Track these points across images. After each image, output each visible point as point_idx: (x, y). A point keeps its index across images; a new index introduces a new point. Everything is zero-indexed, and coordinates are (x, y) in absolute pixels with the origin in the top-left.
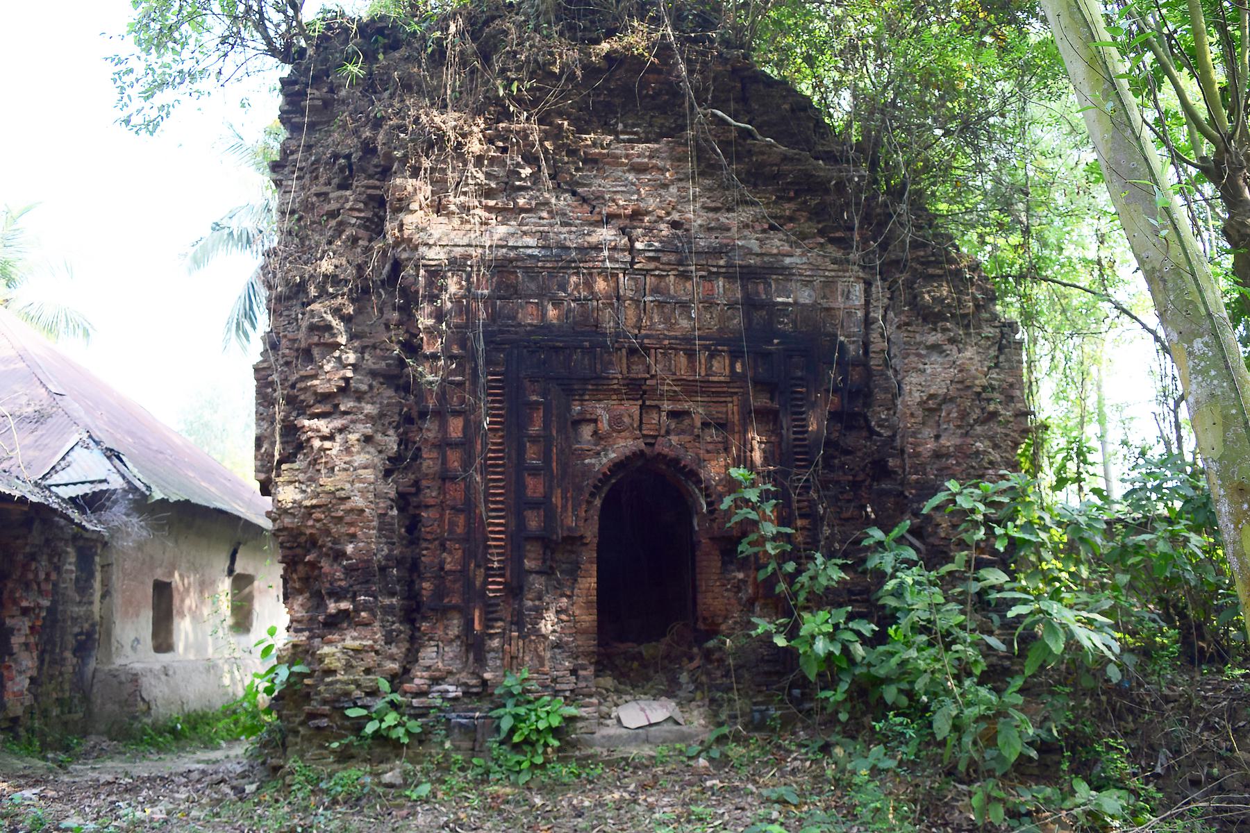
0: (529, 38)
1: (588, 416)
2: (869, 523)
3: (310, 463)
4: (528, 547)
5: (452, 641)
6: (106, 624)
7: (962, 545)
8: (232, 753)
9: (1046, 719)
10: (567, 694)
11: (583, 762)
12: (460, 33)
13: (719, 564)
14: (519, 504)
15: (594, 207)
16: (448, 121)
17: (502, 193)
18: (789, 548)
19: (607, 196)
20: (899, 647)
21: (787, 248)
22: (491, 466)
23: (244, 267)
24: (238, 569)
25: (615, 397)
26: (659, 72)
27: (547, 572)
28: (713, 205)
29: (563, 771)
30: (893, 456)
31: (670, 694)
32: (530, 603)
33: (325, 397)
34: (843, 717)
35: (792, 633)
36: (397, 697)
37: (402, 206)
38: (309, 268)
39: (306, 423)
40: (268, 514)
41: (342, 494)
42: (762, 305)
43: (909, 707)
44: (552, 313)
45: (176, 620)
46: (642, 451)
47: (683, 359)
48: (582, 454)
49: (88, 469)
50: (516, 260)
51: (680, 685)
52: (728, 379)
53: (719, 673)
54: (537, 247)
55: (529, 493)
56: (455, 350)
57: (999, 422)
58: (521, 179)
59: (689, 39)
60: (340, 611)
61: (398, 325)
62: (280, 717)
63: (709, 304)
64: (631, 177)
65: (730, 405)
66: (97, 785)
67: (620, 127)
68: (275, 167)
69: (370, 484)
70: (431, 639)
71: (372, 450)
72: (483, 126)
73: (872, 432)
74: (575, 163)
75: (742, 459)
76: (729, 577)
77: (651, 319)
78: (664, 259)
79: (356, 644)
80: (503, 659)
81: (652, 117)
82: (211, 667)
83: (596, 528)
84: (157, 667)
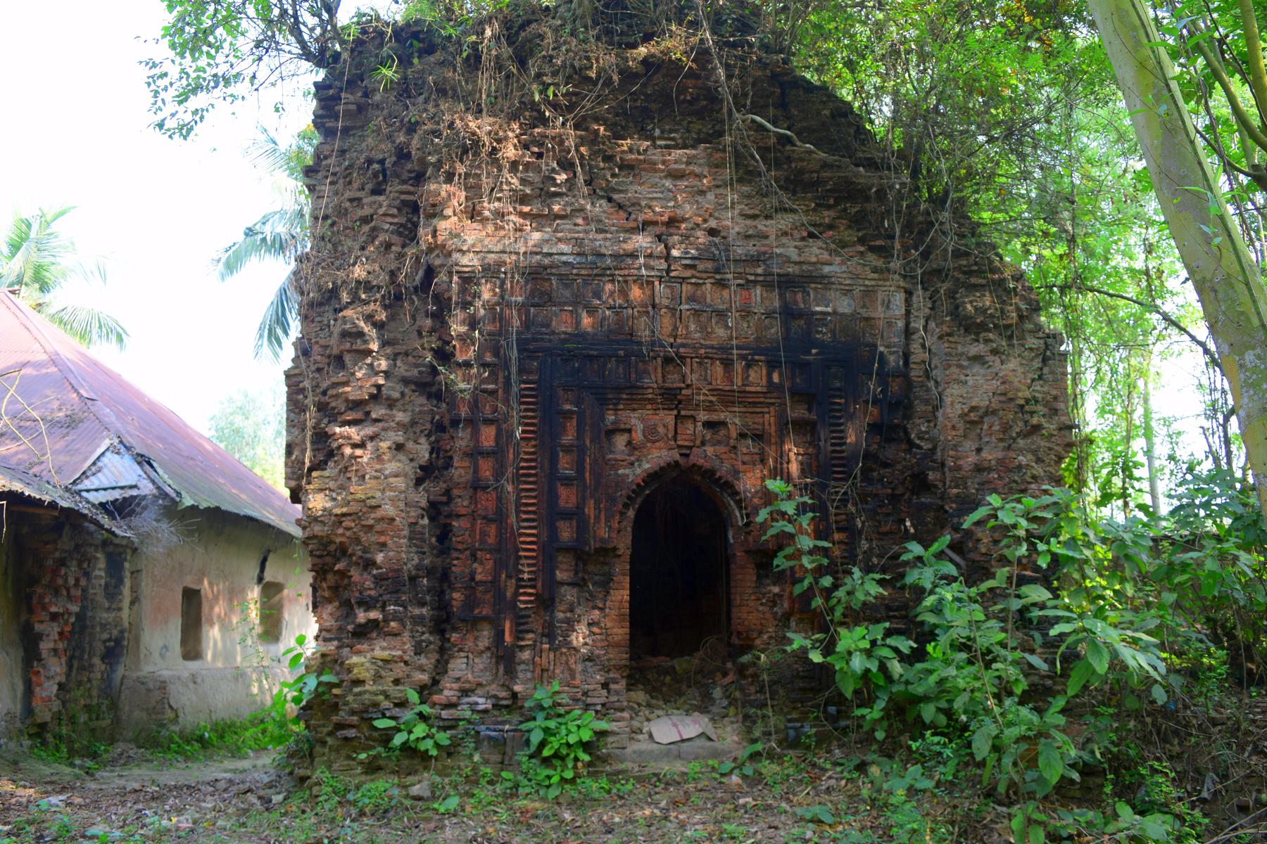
0: (565, 42)
1: (622, 426)
2: (908, 537)
3: (340, 471)
4: (560, 558)
5: (482, 652)
6: (135, 627)
7: (1004, 561)
8: (259, 763)
9: (1089, 740)
10: (599, 708)
11: (614, 777)
14: (552, 514)
16: (482, 126)
17: (537, 199)
18: (825, 562)
19: (643, 203)
21: (826, 256)
23: (275, 272)
24: (268, 577)
26: (697, 77)
27: (579, 584)
28: (751, 212)
29: (593, 786)
30: (933, 469)
31: (703, 709)
32: (561, 615)
33: (357, 404)
34: (880, 735)
35: (829, 649)
36: (426, 709)
37: (436, 212)
38: (341, 274)
39: (338, 430)
41: (373, 502)
42: (800, 315)
44: (586, 321)
45: (205, 628)
46: (676, 462)
47: (719, 369)
48: (616, 465)
49: (119, 473)
50: (551, 267)
51: (713, 701)
52: (765, 390)
53: (753, 689)
54: (572, 254)
55: (562, 503)
56: (489, 358)
57: (1043, 436)
58: (556, 185)
59: (728, 44)
60: (369, 621)
61: (430, 332)
62: (307, 727)
63: (746, 313)
64: (668, 183)
66: (123, 793)
67: (657, 132)
70: (461, 650)
71: (403, 458)
73: (911, 444)
74: (611, 169)
75: (779, 472)
76: (764, 590)
77: (687, 327)
78: (701, 267)
79: (385, 654)
80: (533, 672)
81: (690, 122)
82: (240, 676)
83: (629, 541)
84: (186, 674)
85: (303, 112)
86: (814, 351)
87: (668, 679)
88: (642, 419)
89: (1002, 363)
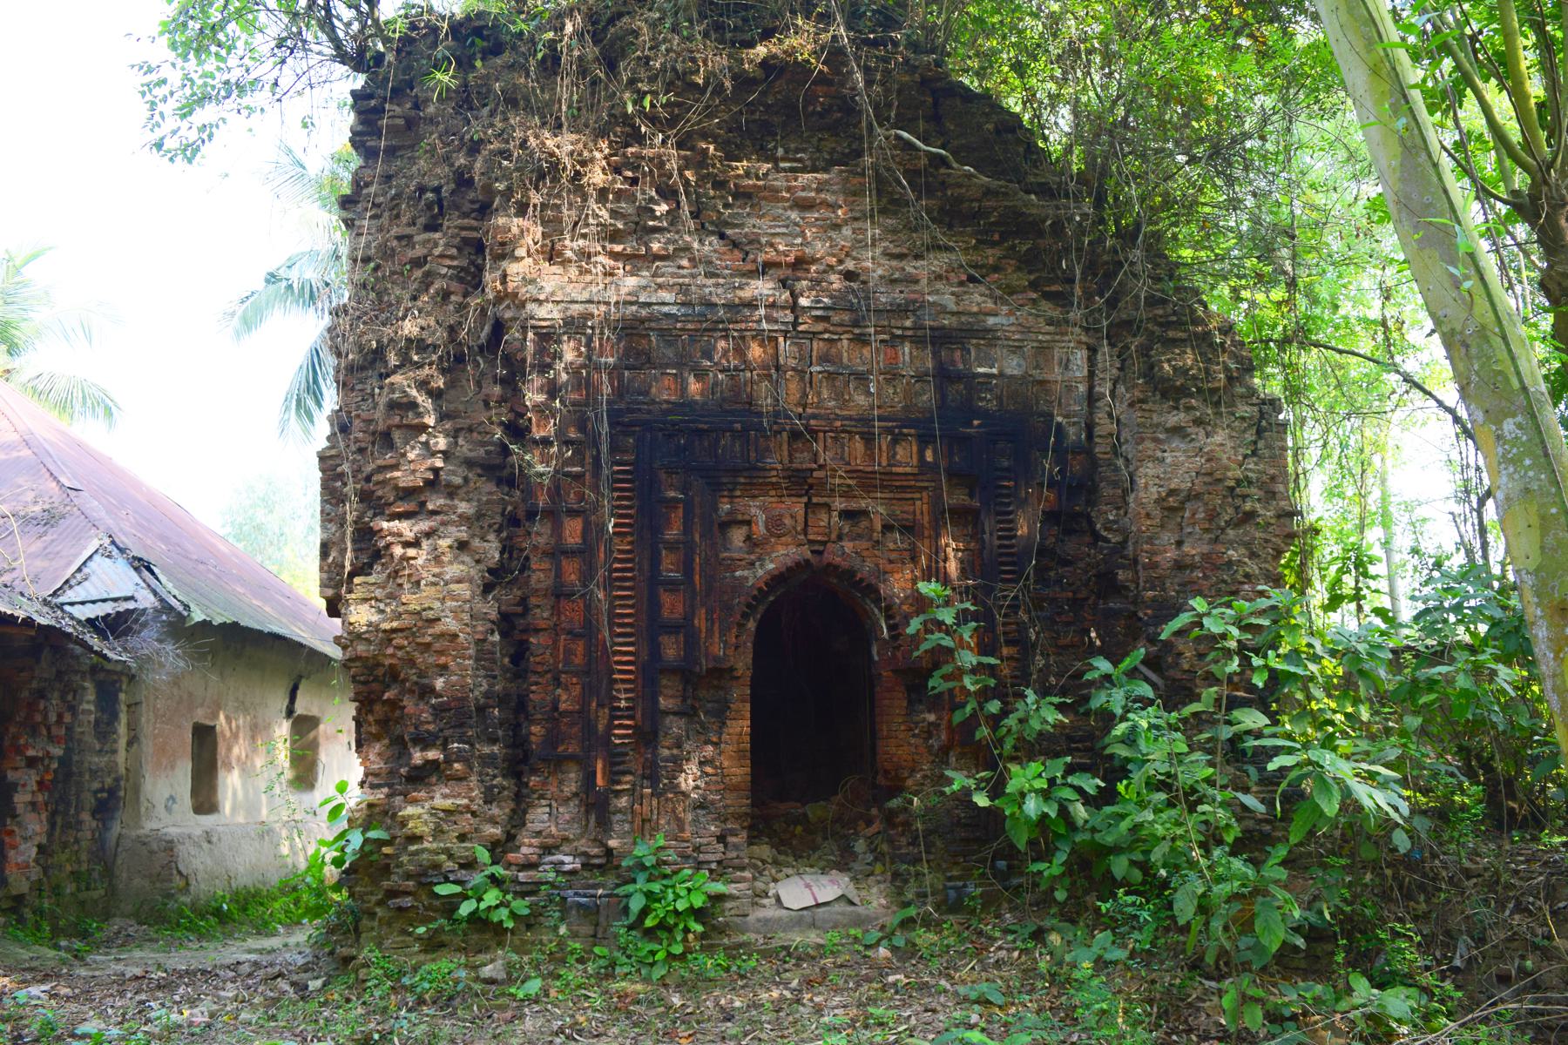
0: (665, 40)
1: (740, 517)
2: (1093, 651)
3: (389, 576)
4: (664, 682)
5: (569, 799)
6: (133, 780)
7: (1211, 679)
8: (292, 940)
9: (1316, 898)
10: (714, 866)
11: (733, 951)
12: (579, 34)
13: (905, 704)
14: (653, 627)
15: (747, 253)
16: (563, 145)
17: (631, 236)
18: (992, 682)
19: (764, 240)
20: (1131, 807)
21: (990, 305)
22: (618, 579)
23: (305, 330)
24: (300, 709)
25: (773, 493)
26: (829, 83)
28: (897, 250)
30: (1123, 567)
31: (843, 867)
32: (666, 752)
33: (408, 493)
34: (1060, 895)
35: (996, 790)
36: (499, 870)
37: (505, 252)
38: (388, 330)
39: (385, 525)
40: (337, 640)
41: (430, 614)
42: (959, 377)
43: (1143, 883)
44: (694, 386)
45: (221, 773)
46: (807, 561)
47: (859, 445)
48: (732, 565)
49: (111, 582)
50: (650, 320)
51: (854, 856)
52: (916, 471)
54: (675, 303)
55: (666, 614)
56: (573, 434)
57: (1257, 525)
58: (655, 218)
59: (867, 42)
60: (427, 762)
62: (352, 895)
63: (892, 375)
64: (794, 215)
65: (918, 503)
66: (121, 981)
67: (780, 152)
68: (346, 203)
69: (465, 602)
70: (542, 797)
71: (467, 559)
72: (607, 151)
73: (1097, 537)
74: (722, 197)
75: (934, 572)
76: (916, 719)
77: (819, 394)
78: (836, 319)
79: (448, 803)
81: (820, 140)
82: (265, 832)
84: (198, 832)
85: (338, 126)
86: (976, 422)
87: (799, 829)
88: (764, 509)
89: (1208, 435)
